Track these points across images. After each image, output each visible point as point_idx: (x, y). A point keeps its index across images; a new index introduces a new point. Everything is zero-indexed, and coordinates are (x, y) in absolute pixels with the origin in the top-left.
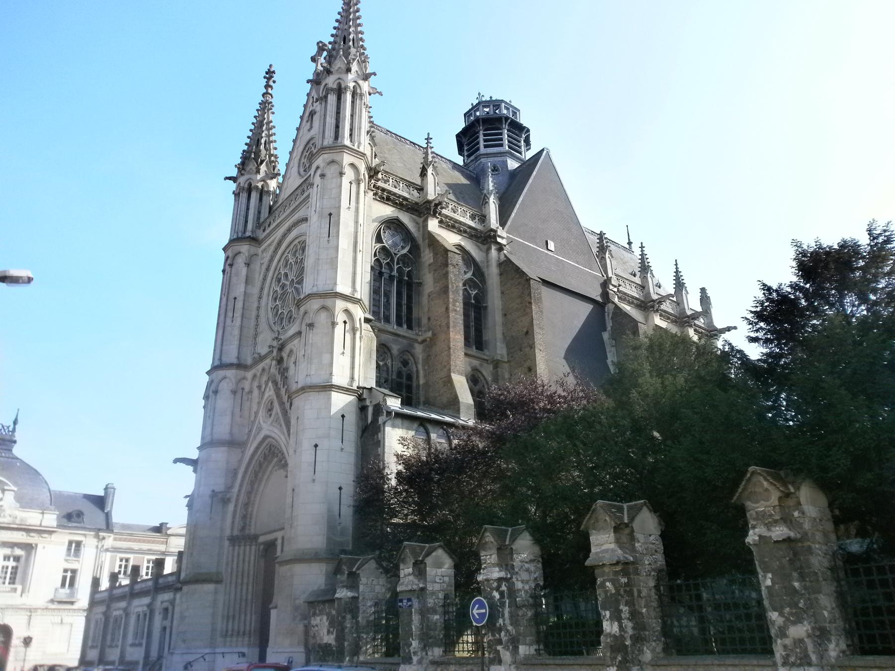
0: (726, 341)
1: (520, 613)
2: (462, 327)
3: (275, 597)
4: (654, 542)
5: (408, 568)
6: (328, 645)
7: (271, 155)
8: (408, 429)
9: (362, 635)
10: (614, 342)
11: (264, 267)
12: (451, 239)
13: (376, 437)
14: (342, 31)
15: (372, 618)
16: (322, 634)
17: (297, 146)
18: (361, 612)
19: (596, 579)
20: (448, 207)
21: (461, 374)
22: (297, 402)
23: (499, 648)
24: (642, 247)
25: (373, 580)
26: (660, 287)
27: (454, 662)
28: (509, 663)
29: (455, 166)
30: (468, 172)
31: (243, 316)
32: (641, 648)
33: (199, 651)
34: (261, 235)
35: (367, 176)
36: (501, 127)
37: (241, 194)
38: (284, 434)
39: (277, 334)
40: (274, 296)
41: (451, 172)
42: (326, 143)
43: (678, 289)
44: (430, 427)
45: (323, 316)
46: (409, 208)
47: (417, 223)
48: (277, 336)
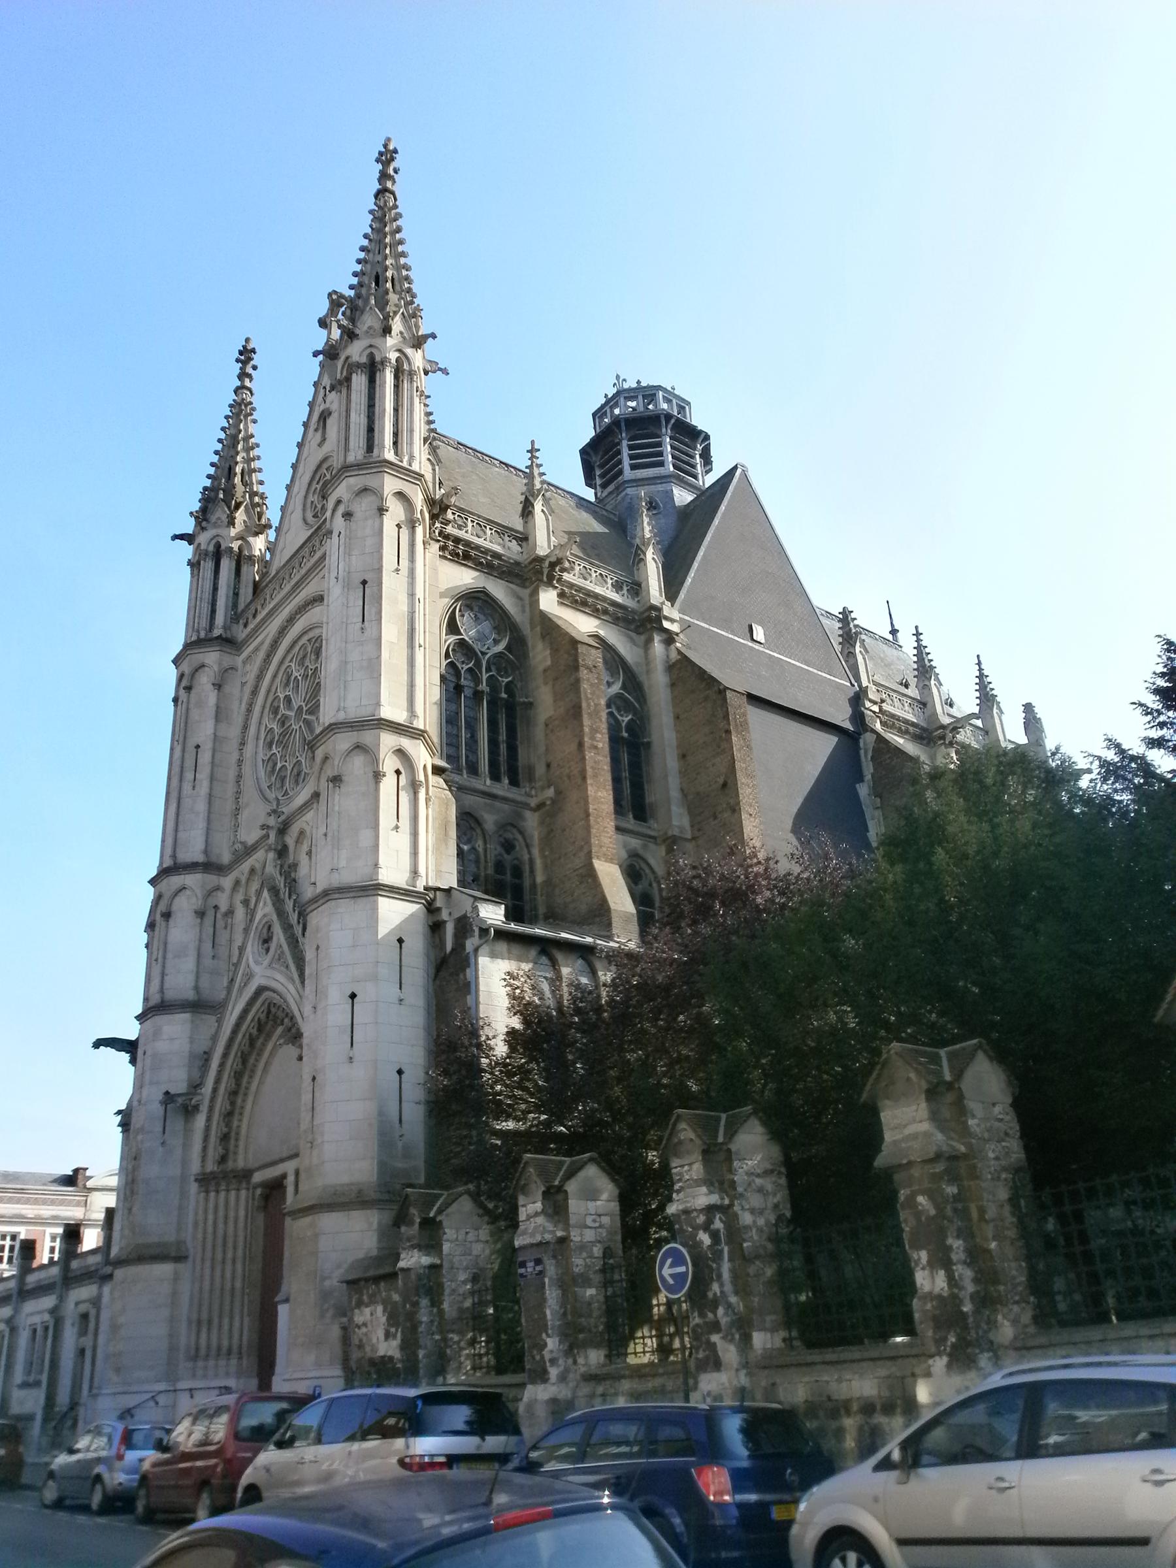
0: (1110, 740)
1: (752, 1270)
2: (609, 777)
3: (285, 1281)
4: (1001, 1116)
5: (534, 1203)
6: (387, 1360)
7: (253, 494)
8: (520, 959)
9: (451, 1335)
10: (878, 800)
11: (248, 689)
12: (583, 625)
13: (461, 976)
14: (373, 265)
15: (468, 1303)
16: (374, 1341)
17: (299, 475)
18: (447, 1292)
19: (895, 1193)
20: (573, 569)
21: (611, 861)
22: (314, 919)
23: (715, 1338)
24: (918, 634)
25: (467, 1233)
26: (951, 705)
27: (627, 1373)
28: (735, 1366)
29: (581, 502)
30: (604, 512)
31: (212, 778)
32: (992, 1318)
33: (146, 1387)
34: (240, 633)
35: (427, 516)
36: (659, 432)
37: (202, 562)
38: (292, 980)
39: (275, 803)
40: (268, 739)
41: (574, 512)
42: (351, 458)
43: (984, 707)
44: (560, 956)
45: (358, 762)
46: (503, 572)
47: (520, 599)
48: (275, 807)
